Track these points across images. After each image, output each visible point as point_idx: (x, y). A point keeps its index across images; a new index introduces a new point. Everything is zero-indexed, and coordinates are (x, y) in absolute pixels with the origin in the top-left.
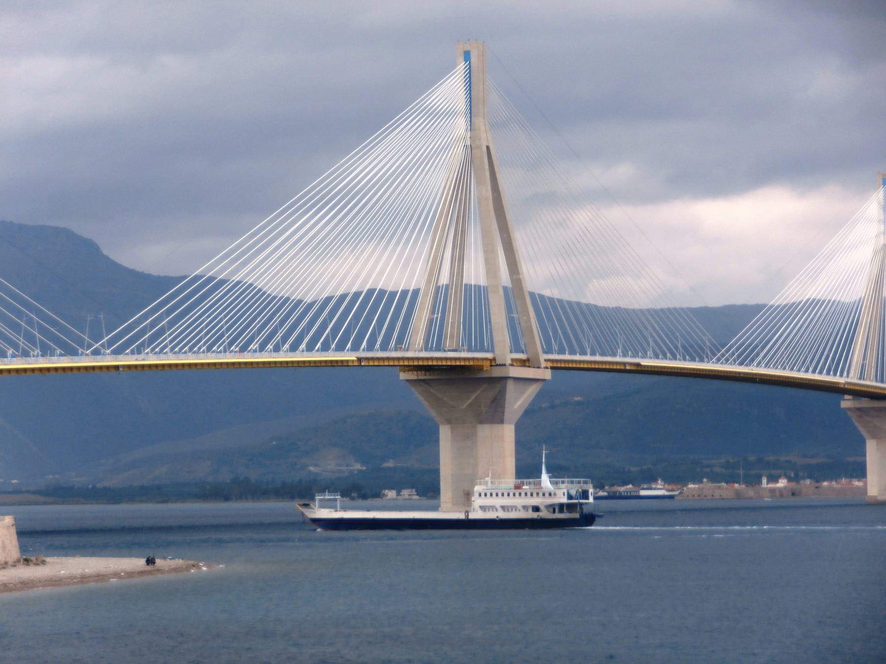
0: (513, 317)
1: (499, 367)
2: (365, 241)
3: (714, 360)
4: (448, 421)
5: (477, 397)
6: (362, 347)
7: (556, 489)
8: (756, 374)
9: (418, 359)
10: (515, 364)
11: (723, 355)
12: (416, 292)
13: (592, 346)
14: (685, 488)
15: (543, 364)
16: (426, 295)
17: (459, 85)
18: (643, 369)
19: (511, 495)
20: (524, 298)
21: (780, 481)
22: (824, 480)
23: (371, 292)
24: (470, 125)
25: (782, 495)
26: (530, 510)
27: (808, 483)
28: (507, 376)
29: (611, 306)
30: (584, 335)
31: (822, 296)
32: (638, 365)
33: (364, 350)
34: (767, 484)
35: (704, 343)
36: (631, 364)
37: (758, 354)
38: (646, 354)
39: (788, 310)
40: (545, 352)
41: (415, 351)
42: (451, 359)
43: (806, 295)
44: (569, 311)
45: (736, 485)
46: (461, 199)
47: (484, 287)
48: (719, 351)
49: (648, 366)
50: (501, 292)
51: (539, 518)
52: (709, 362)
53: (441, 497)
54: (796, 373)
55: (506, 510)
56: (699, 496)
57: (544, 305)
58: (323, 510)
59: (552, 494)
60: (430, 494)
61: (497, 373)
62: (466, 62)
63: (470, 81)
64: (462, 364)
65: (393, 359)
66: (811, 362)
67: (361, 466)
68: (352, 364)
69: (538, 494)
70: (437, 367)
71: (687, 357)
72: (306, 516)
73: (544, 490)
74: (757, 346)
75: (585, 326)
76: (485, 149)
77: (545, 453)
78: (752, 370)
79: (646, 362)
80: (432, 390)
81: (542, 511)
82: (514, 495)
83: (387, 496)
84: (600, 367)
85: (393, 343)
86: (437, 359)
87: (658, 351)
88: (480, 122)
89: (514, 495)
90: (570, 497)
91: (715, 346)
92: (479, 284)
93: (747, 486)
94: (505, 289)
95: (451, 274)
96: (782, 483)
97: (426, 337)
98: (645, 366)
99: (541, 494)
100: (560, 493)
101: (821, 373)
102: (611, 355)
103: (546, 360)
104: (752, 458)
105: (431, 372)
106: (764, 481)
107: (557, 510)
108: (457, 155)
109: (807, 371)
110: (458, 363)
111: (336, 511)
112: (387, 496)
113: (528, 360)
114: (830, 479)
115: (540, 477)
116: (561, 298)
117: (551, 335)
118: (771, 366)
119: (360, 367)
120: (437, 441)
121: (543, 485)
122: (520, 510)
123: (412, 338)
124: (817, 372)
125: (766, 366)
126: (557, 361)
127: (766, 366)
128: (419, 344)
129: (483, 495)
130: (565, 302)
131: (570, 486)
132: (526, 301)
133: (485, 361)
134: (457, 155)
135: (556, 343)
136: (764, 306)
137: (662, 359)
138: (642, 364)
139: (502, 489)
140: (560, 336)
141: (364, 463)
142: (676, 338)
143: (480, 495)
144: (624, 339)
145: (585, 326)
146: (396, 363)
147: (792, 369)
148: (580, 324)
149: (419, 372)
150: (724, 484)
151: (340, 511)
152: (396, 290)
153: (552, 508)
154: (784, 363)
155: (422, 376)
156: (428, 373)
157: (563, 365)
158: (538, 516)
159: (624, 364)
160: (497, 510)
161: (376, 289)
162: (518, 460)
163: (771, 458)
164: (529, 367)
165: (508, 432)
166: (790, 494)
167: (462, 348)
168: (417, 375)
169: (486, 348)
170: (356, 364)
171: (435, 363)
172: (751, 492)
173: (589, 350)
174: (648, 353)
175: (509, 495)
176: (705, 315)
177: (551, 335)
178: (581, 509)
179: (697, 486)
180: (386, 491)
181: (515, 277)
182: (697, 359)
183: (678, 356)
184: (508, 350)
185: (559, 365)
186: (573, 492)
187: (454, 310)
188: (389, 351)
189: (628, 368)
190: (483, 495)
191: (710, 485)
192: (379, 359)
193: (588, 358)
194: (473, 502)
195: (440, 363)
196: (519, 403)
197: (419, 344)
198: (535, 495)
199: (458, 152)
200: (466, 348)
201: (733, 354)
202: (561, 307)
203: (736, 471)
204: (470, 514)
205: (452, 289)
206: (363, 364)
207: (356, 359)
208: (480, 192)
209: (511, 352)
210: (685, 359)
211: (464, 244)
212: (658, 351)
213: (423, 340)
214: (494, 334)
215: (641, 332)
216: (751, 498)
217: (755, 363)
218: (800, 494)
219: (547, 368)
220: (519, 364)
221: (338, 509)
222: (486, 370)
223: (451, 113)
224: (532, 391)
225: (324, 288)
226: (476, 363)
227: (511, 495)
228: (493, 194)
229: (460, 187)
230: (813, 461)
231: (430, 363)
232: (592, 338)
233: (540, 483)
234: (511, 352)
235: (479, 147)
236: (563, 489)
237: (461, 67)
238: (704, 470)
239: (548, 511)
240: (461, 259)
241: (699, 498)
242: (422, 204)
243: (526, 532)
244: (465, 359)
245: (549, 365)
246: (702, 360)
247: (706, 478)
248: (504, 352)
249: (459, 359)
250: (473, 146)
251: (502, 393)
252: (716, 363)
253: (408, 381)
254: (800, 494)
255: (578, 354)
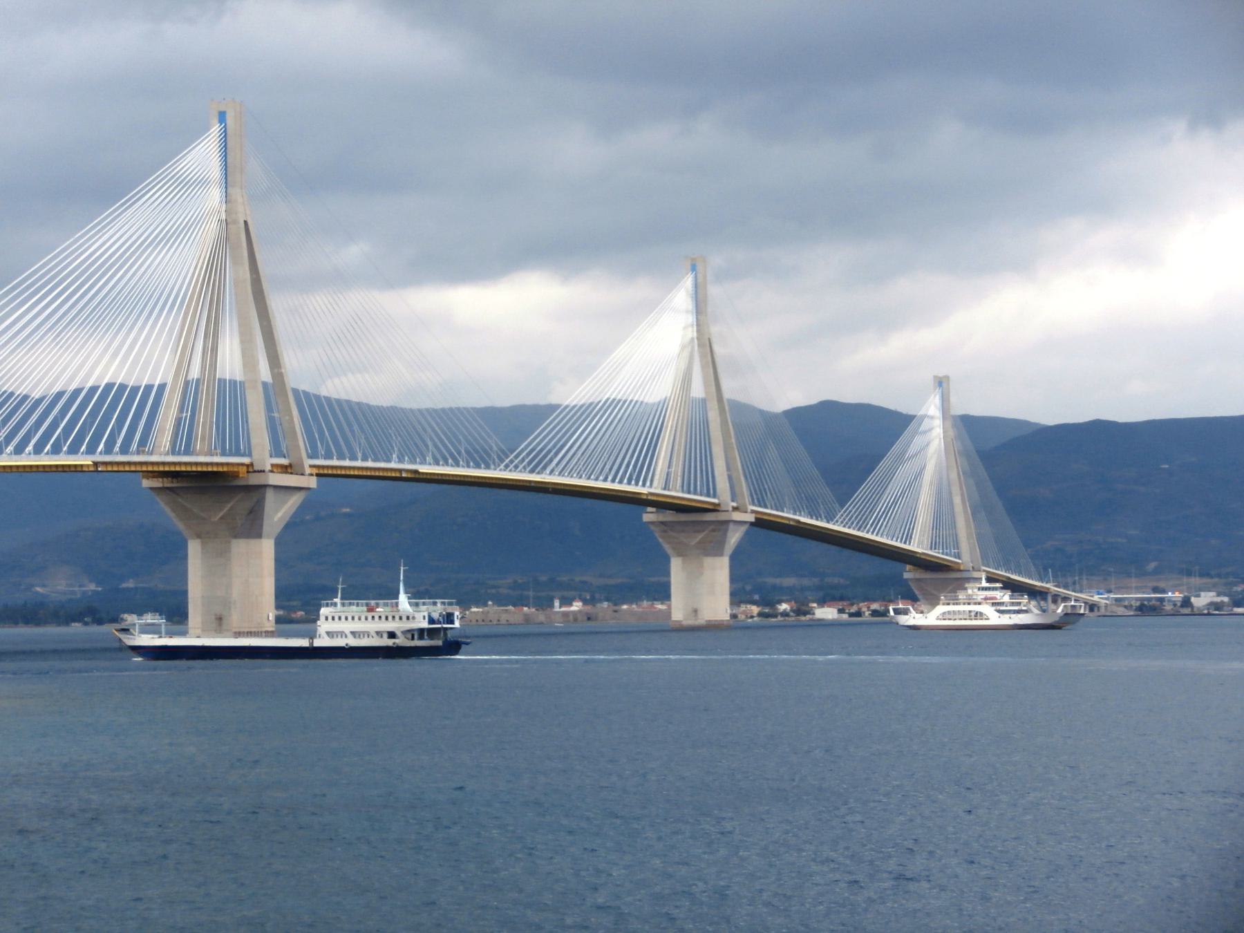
0: (274, 417)
1: (257, 474)
2: (100, 332)
3: (502, 466)
4: (199, 536)
5: (231, 508)
6: (99, 450)
7: (416, 611)
8: (549, 483)
9: (164, 464)
10: (275, 470)
11: (512, 462)
12: (162, 387)
13: (364, 450)
14: (467, 612)
15: (308, 471)
16: (172, 391)
17: (213, 151)
18: (421, 476)
19: (363, 618)
20: (286, 396)
21: (575, 604)
22: (623, 603)
23: (109, 386)
24: (226, 197)
25: (576, 620)
26: (385, 636)
27: (606, 606)
28: (266, 483)
29: (385, 405)
30: (354, 437)
31: (101, 377)
32: (416, 472)
33: (101, 453)
34: (560, 607)
35: (491, 448)
36: (407, 471)
37: (551, 460)
38: (425, 460)
39: (571, 411)
40: (310, 457)
41: (161, 455)
42: (201, 464)
43: (604, 396)
44: (338, 411)
45: (525, 609)
46: (214, 281)
47: (240, 382)
48: (507, 457)
49: (427, 474)
50: (261, 388)
51: (395, 646)
52: (495, 469)
53: (189, 623)
54: (593, 482)
55: (331, 636)
56: (483, 621)
57: (313, 406)
58: (144, 636)
59: (411, 617)
60: (175, 619)
61: (254, 480)
62: (221, 125)
63: (225, 146)
64: (215, 469)
65: (135, 464)
66: (611, 469)
67: (97, 587)
68: (87, 470)
69: (394, 617)
70: (195, 474)
71: (472, 464)
72: (124, 643)
73: (401, 613)
74: (550, 451)
75: (356, 427)
76: (243, 223)
77: (404, 571)
78: (544, 479)
79: (424, 469)
80: (180, 500)
81: (398, 638)
82: (366, 619)
83: (126, 621)
84: (373, 474)
85: (117, 449)
86: (186, 464)
87: (438, 456)
88: (236, 192)
89: (366, 619)
90: (431, 621)
91: (503, 451)
92: (235, 379)
93: (537, 610)
94: (265, 384)
95: (202, 365)
96: (577, 606)
97: (173, 439)
98: (423, 473)
99: (397, 618)
100: (419, 616)
101: (621, 482)
102: (385, 461)
103: (311, 466)
104: (544, 578)
105: (179, 479)
106: (557, 603)
107: (416, 637)
108: (211, 229)
109: (605, 480)
110: (210, 469)
111: (161, 637)
112: (126, 621)
113: (290, 466)
114: (630, 602)
115: (397, 598)
116: (329, 396)
117: (317, 436)
118: (566, 474)
119: (96, 473)
120: (185, 557)
121: (400, 607)
122: (373, 637)
123: (157, 440)
124: (617, 481)
125: (559, 474)
126: (323, 467)
127: (559, 474)
128: (165, 447)
129: (330, 618)
130: (333, 400)
131: (432, 608)
132: (288, 399)
133: (241, 467)
134: (211, 229)
135: (322, 445)
136: (558, 406)
137: (443, 465)
138: (421, 471)
139: (352, 612)
140: (327, 438)
141: (98, 584)
142: (460, 443)
143: (327, 618)
144: (399, 442)
145: (356, 427)
146: (139, 468)
147: (589, 478)
148: (350, 425)
149: (165, 479)
150: (511, 608)
151: (165, 637)
152: (139, 385)
153: (411, 633)
154: (580, 470)
155: (167, 483)
156: (175, 480)
157: (330, 472)
158: (394, 643)
159: (400, 471)
160: (346, 637)
161: (140, 387)
162: (277, 580)
163: (564, 578)
164: (291, 473)
165: (266, 548)
166: (586, 618)
167: (215, 451)
168: (163, 482)
169: (242, 451)
170: (92, 469)
171: (183, 469)
172: (541, 617)
173: (360, 455)
174: (427, 458)
175: (360, 619)
176: (491, 415)
177: (317, 436)
178: (445, 634)
179: (481, 610)
180: (126, 616)
181: (276, 371)
182: (483, 466)
183: (461, 463)
184: (268, 454)
185: (326, 472)
186: (435, 616)
187: (206, 407)
188: (131, 454)
189: (404, 475)
190: (330, 618)
191: (496, 608)
192: (118, 464)
193: (359, 463)
194: (318, 628)
195: (189, 469)
196: (280, 515)
197: (165, 447)
198: (390, 618)
199: (210, 230)
200: (219, 451)
201: (523, 460)
202: (328, 405)
203: (525, 593)
204: (315, 640)
205: (203, 384)
206: (100, 469)
207: (91, 463)
208: (236, 273)
209: (271, 456)
210: (468, 466)
211: (218, 337)
212: (438, 456)
213: (170, 442)
214: (252, 435)
215: (419, 435)
216: (542, 623)
217: (548, 471)
218: (596, 619)
219: (312, 475)
220: (279, 470)
221: (163, 635)
222: (242, 477)
223: (204, 182)
224: (294, 501)
225: (573, 401)
226: (231, 469)
227: (363, 618)
228: (251, 275)
229: (214, 268)
230: (611, 582)
231: (178, 469)
232: (363, 441)
233: (397, 604)
234: (271, 456)
235: (235, 222)
236: (424, 611)
237: (216, 129)
238: (489, 591)
239: (406, 637)
240: (215, 350)
241: (483, 623)
242: (170, 286)
243: (380, 661)
244: (217, 464)
245: (315, 471)
246: (488, 467)
247: (492, 601)
248: (263, 456)
249: (212, 464)
250: (229, 220)
251: (260, 504)
252: (505, 470)
253: (151, 488)
254: (596, 619)
255: (370, 459)
